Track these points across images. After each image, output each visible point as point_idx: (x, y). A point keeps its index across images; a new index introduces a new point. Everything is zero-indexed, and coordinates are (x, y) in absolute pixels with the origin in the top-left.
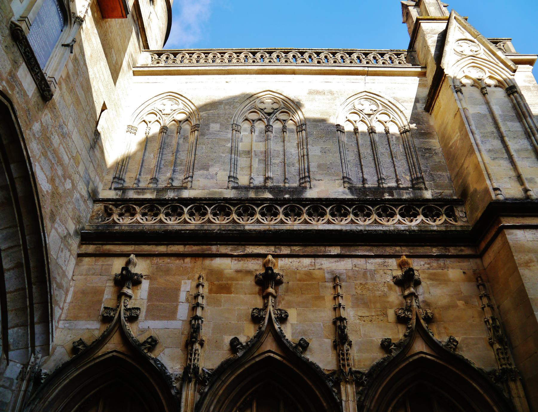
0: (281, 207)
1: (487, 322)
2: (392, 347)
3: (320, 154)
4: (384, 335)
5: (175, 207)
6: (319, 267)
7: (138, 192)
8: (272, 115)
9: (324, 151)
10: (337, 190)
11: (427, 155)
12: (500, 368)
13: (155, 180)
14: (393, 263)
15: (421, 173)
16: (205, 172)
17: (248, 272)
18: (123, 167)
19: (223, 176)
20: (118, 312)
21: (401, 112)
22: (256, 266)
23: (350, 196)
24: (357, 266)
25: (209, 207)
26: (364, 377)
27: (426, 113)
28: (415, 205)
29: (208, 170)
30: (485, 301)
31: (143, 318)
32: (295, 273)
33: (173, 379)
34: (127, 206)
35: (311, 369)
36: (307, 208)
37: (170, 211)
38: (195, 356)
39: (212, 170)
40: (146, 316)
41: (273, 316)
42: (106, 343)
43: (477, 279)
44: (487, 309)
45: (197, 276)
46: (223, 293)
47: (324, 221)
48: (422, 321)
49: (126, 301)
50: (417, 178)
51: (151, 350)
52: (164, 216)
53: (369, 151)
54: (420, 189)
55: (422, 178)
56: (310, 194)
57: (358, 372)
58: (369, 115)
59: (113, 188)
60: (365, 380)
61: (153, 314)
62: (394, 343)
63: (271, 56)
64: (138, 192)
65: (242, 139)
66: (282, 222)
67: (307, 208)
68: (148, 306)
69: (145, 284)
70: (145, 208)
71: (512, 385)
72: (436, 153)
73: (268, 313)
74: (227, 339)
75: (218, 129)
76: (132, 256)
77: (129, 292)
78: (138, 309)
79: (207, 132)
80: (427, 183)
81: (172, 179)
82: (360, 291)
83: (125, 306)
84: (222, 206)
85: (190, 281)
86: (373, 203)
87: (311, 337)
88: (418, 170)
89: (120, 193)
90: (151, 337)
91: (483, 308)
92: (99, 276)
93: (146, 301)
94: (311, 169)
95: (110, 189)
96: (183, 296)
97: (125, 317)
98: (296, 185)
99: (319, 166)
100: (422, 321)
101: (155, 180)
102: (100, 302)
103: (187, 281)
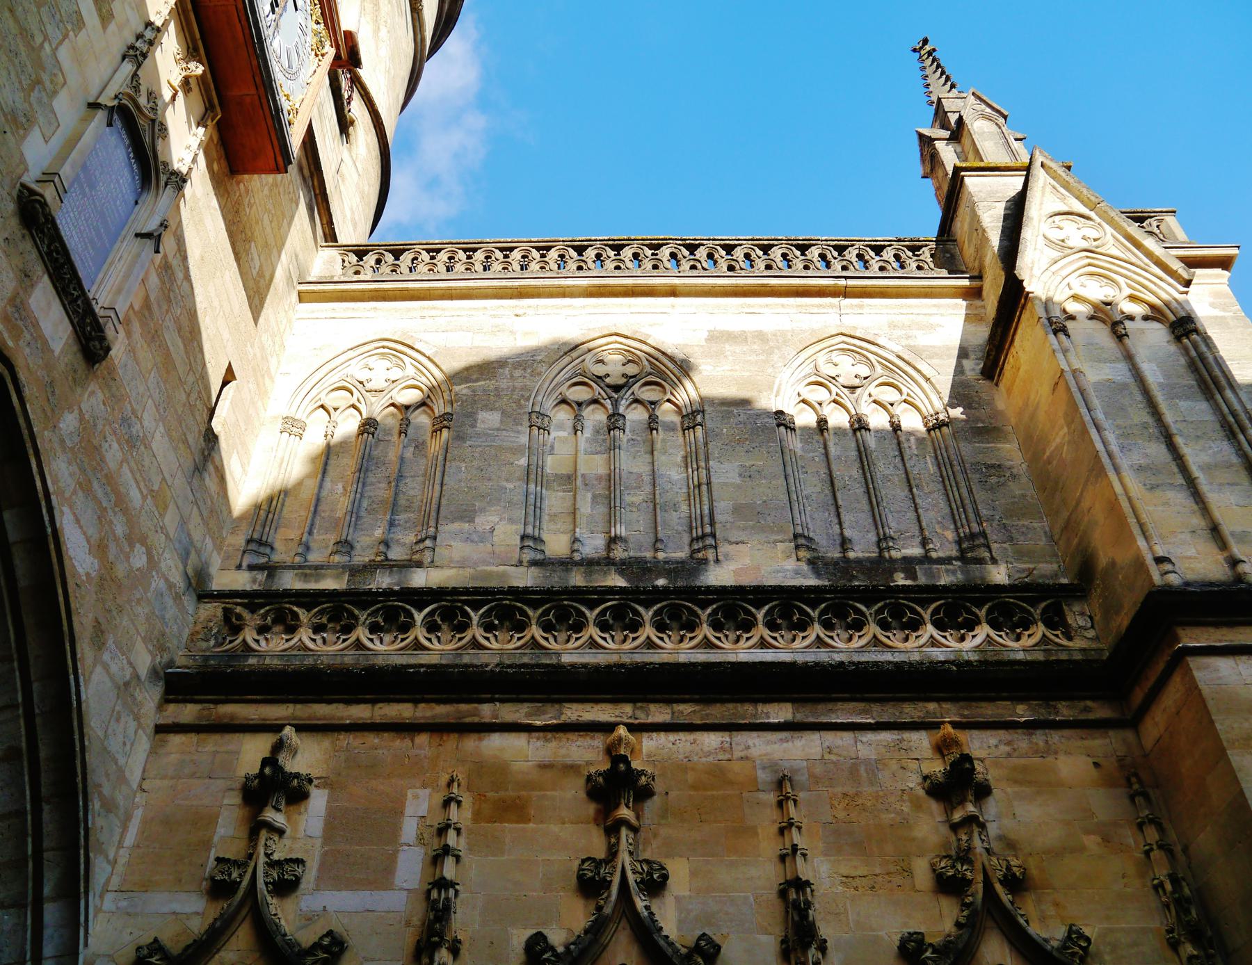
1: (1159, 887)
2: (928, 954)
3: (738, 481)
5: (393, 610)
6: (743, 754)
9: (747, 474)
10: (777, 566)
11: (993, 480)
13: (345, 546)
17: (571, 769)
18: (270, 516)
19: (507, 534)
20: (250, 870)
21: (928, 380)
23: (812, 581)
24: (835, 751)
25: (476, 609)
27: (987, 383)
29: (471, 521)
30: (1152, 834)
31: (312, 886)
34: (278, 608)
36: (709, 610)
37: (380, 619)
39: (484, 521)
40: (318, 878)
42: (219, 950)
43: (1128, 780)
44: (1156, 854)
45: (445, 778)
46: (509, 821)
48: (998, 887)
50: (973, 536)
53: (855, 472)
54: (980, 561)
55: (983, 534)
56: (719, 576)
58: (853, 388)
59: (245, 564)
61: (334, 875)
65: (552, 447)
67: (709, 610)
69: (318, 800)
70: (321, 612)
72: (1014, 476)
76: (288, 730)
77: (278, 819)
78: (299, 862)
80: (994, 546)
81: (386, 543)
83: (267, 855)
84: (505, 607)
85: (428, 791)
87: (724, 931)
88: (972, 516)
89: (261, 576)
90: (330, 933)
91: (1147, 853)
93: (319, 842)
95: (239, 567)
96: (409, 829)
97: (266, 884)
98: (682, 554)
99: (738, 510)
100: (998, 887)
101: (345, 546)
102: (207, 845)
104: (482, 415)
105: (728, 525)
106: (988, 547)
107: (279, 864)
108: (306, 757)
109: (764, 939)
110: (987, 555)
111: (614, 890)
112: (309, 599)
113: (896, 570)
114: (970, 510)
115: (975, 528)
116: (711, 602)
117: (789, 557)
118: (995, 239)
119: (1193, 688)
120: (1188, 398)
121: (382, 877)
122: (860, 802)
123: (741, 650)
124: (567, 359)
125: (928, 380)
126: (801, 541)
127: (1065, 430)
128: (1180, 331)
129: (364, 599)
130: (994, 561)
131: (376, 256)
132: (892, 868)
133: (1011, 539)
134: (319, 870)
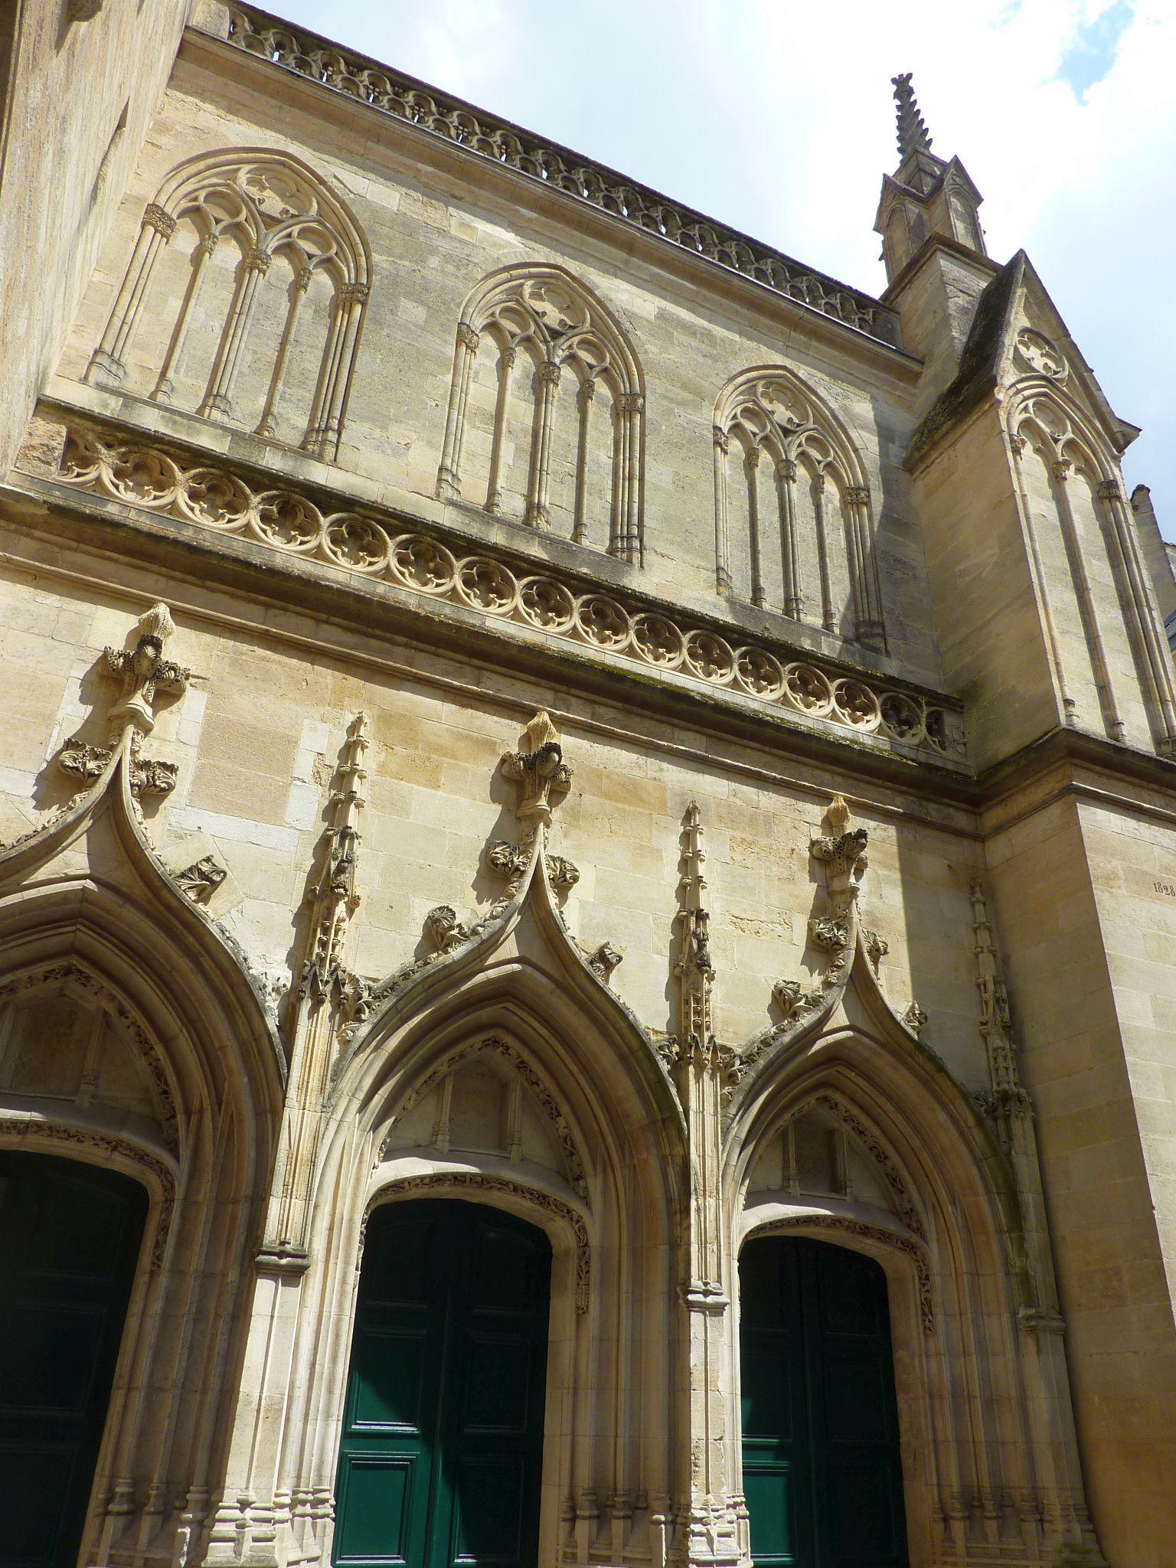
0: (325, 514)
1: (981, 986)
2: (802, 1003)
3: (671, 487)
4: (781, 973)
5: (295, 503)
6: (656, 775)
7: (175, 422)
8: (562, 340)
9: (681, 484)
10: (696, 594)
11: (898, 574)
12: (995, 1087)
14: (816, 812)
15: (880, 613)
16: (378, 432)
17: (489, 745)
18: (126, 328)
19: (424, 460)
20: (113, 764)
21: (856, 450)
22: (508, 734)
23: (729, 619)
24: (739, 795)
25: (392, 535)
26: (738, 1062)
27: (907, 475)
28: (379, 522)
29: (384, 428)
30: (984, 937)
31: (184, 800)
32: (600, 775)
33: (269, 989)
34: (144, 454)
35: (612, 1019)
36: (637, 618)
37: (275, 508)
38: (336, 935)
41: (546, 873)
42: (64, 849)
43: (972, 888)
44: (986, 957)
45: (350, 718)
46: (417, 782)
47: (562, 628)
48: (866, 956)
49: (138, 738)
50: (871, 624)
51: (204, 895)
52: (111, 472)
53: (776, 518)
54: (875, 650)
55: (882, 625)
56: (640, 582)
57: (726, 1050)
58: (787, 432)
59: (92, 379)
60: (740, 1071)
62: (805, 996)
63: (569, 172)
64: (175, 422)
65: (477, 373)
66: (318, 553)
67: (637, 618)
68: (200, 768)
69: (193, 703)
71: (1017, 1126)
72: (915, 577)
73: (534, 861)
74: (422, 909)
75: (421, 322)
78: (172, 769)
79: (389, 317)
80: (890, 640)
82: (741, 857)
83: (133, 753)
84: (428, 546)
85: (327, 726)
86: (581, 585)
87: (623, 944)
88: (874, 604)
91: (977, 955)
92: (49, 641)
94: (647, 521)
95: (84, 380)
96: (304, 765)
97: (132, 785)
99: (666, 519)
100: (866, 956)
103: (319, 725)
104: (405, 304)
105: (657, 533)
106: (884, 637)
107: (145, 765)
108: (182, 647)
109: (658, 958)
110: (882, 645)
111: (527, 880)
112: (191, 456)
113: (803, 634)
114: (873, 596)
115: (875, 617)
116: (639, 611)
117: (711, 587)
118: (959, 334)
119: (1073, 824)
120: (1099, 559)
121: (270, 809)
122: (756, 850)
123: (665, 669)
124: (505, 275)
125: (856, 450)
126: (721, 577)
127: (997, 550)
128: (1105, 493)
129: (260, 479)
130: (888, 654)
131: (326, 58)
132: (776, 918)
133: (905, 638)
134: (194, 784)
